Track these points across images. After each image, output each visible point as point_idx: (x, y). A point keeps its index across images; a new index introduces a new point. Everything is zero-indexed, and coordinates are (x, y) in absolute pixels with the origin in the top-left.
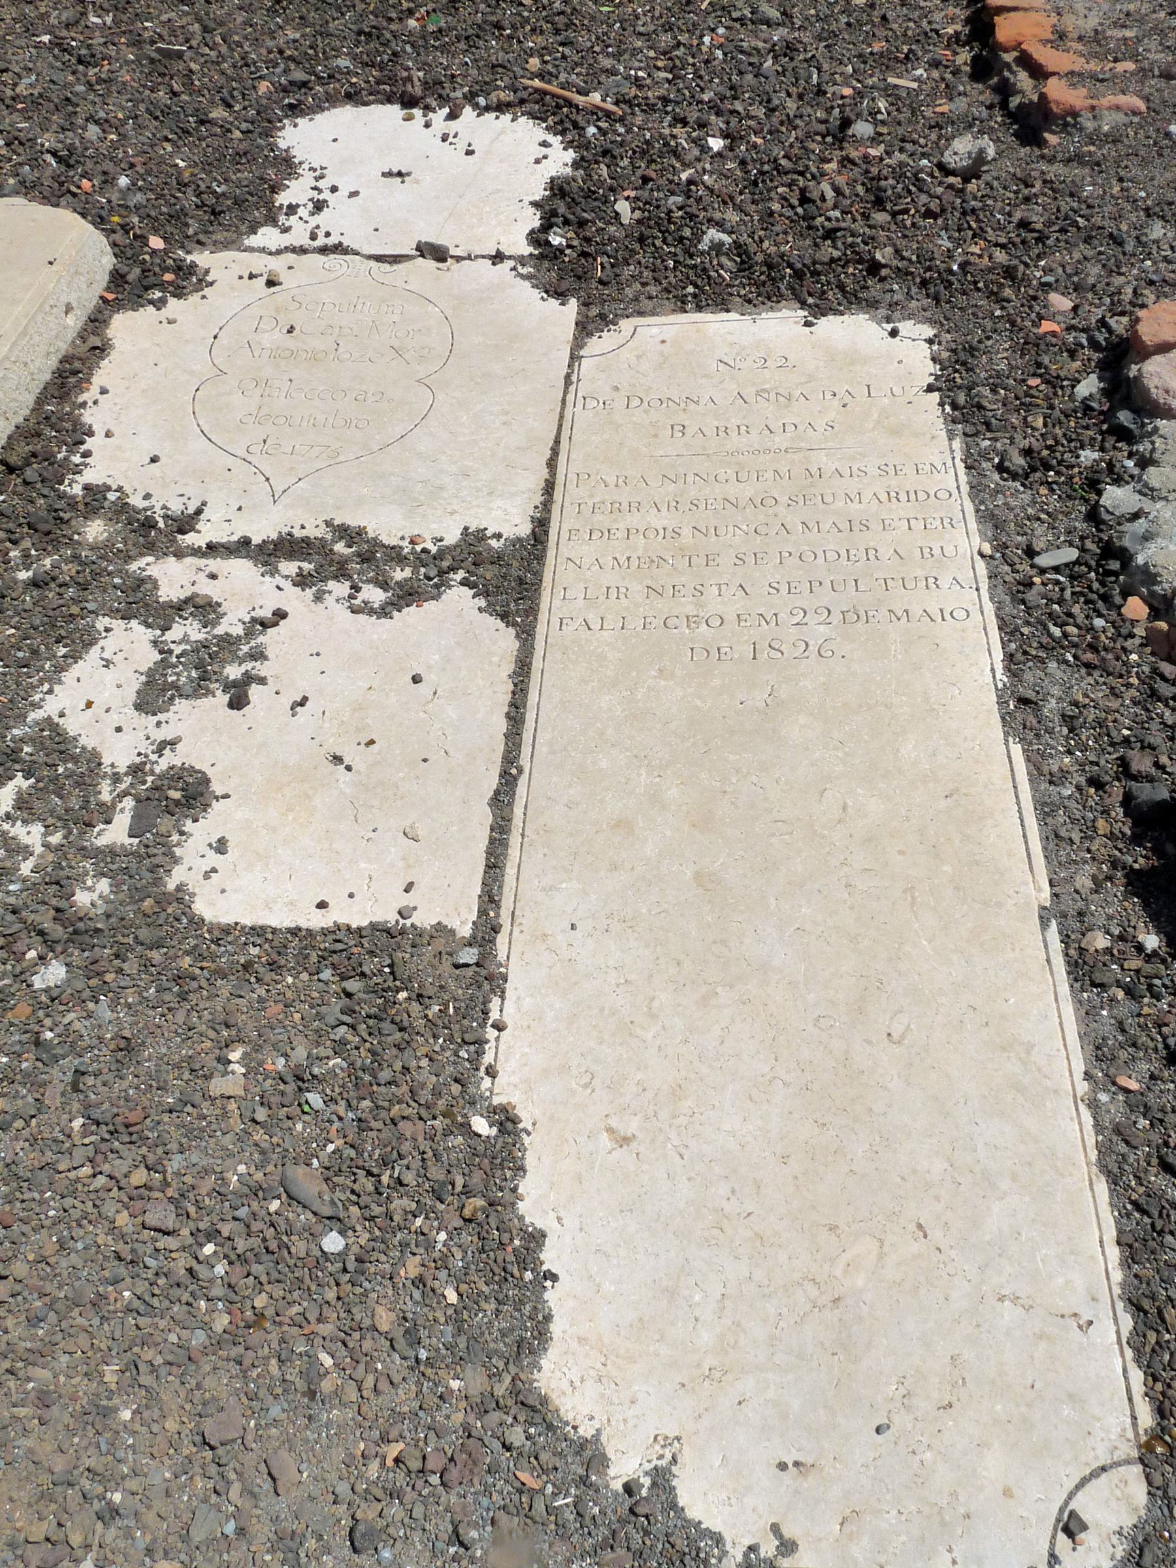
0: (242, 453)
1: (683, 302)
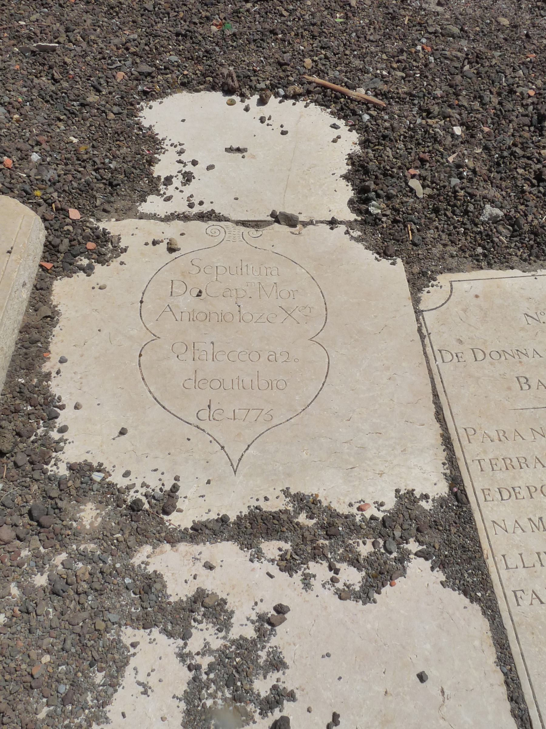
0: (193, 420)
1: (478, 260)
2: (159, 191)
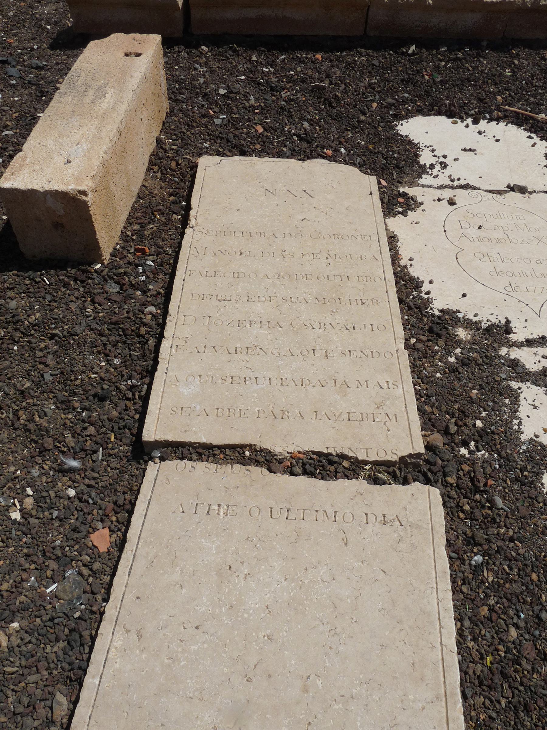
2: (428, 172)
